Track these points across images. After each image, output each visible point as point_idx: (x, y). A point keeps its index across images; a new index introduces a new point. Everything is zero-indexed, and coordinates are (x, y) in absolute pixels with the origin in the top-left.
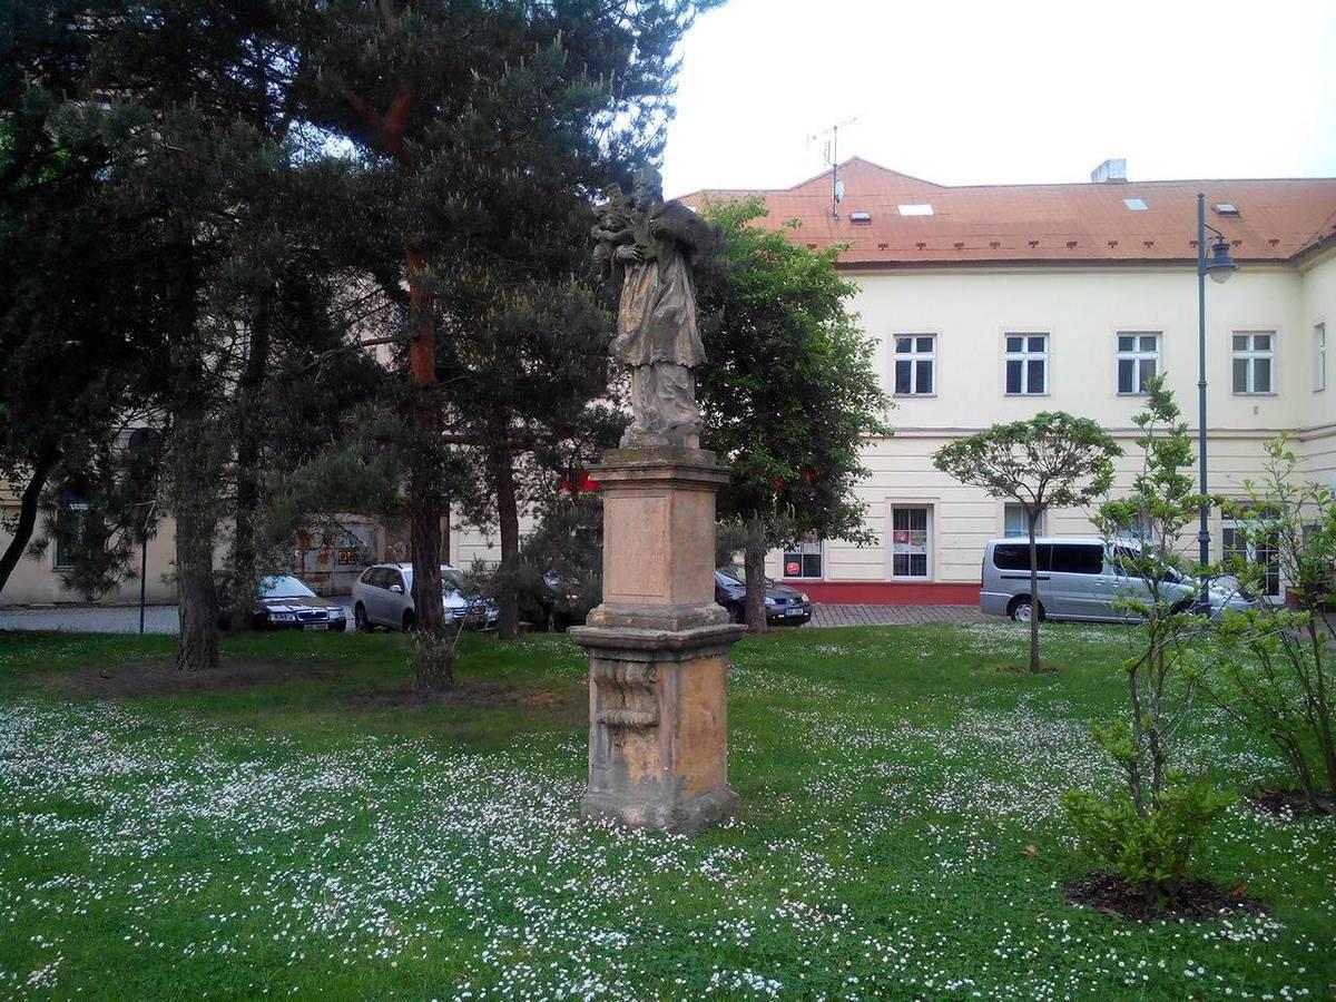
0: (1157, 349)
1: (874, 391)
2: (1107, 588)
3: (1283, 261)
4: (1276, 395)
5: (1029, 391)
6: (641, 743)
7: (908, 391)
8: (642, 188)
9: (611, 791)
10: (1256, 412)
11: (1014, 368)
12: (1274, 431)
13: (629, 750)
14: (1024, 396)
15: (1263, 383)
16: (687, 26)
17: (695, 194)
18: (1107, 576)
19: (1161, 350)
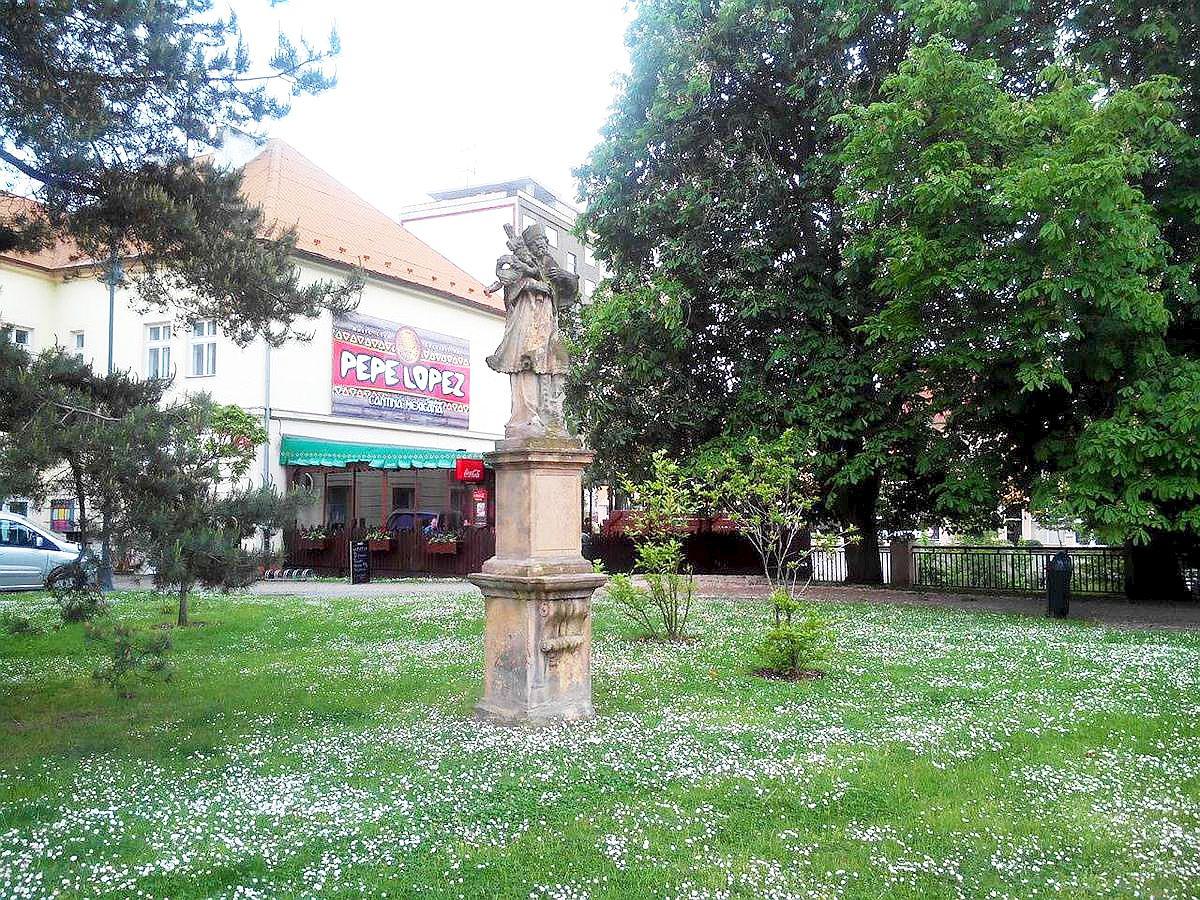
3: (48, 270)
13: (562, 667)
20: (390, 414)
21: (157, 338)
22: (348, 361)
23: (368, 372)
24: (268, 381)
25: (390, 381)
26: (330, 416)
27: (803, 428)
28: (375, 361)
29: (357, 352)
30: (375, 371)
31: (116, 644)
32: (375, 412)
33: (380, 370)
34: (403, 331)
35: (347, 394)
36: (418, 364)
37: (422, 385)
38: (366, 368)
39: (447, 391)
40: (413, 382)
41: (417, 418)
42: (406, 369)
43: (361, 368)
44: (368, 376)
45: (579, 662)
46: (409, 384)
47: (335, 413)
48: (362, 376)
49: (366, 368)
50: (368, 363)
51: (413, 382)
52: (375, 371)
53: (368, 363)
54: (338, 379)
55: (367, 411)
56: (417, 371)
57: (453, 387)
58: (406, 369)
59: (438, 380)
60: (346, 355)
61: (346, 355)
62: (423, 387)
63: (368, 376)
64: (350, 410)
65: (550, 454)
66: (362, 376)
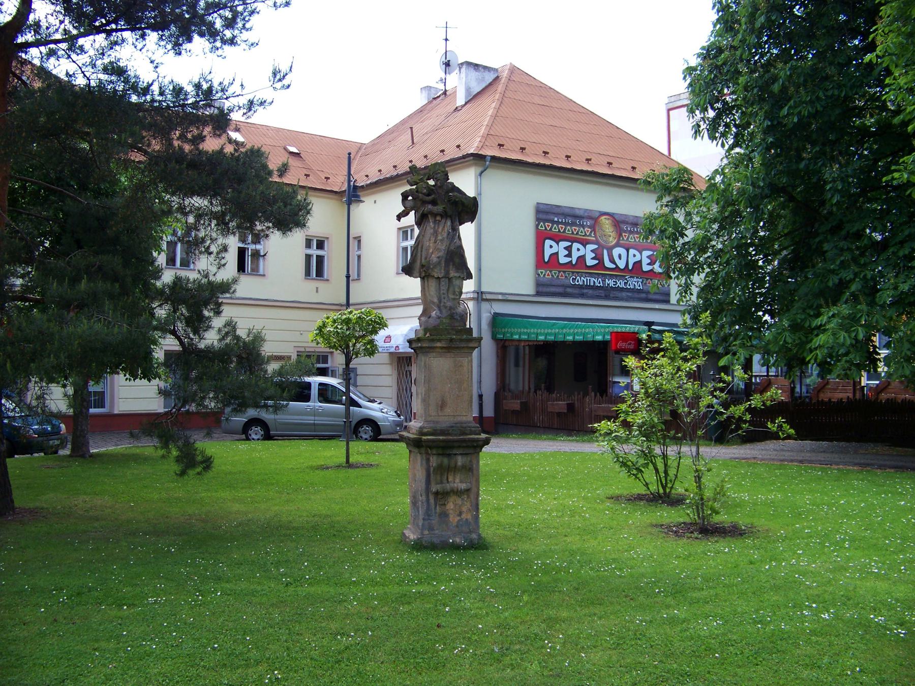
0: (326, 249)
1: (865, 294)
2: (314, 412)
3: (336, 192)
4: (328, 280)
5: (181, 266)
6: (459, 501)
7: (174, 265)
8: (442, 174)
9: (437, 532)
10: (317, 291)
11: (308, 257)
12: (330, 304)
13: (450, 506)
14: (178, 269)
15: (320, 273)
16: (684, 78)
17: (679, 164)
18: (315, 404)
19: (328, 248)
20: (590, 292)
21: (407, 239)
22: (550, 247)
23: (569, 255)
24: (480, 270)
25: (590, 262)
26: (533, 296)
27: (318, 332)
28: (576, 246)
29: (557, 239)
30: (575, 255)
31: (842, 596)
32: (566, 292)
33: (581, 253)
34: (603, 218)
35: (547, 275)
36: (618, 245)
37: (622, 265)
38: (567, 253)
39: (646, 268)
40: (612, 261)
41: (619, 294)
42: (605, 252)
43: (563, 253)
44: (569, 259)
45: (468, 504)
46: (608, 264)
47: (538, 294)
48: (563, 260)
49: (567, 253)
50: (569, 249)
51: (612, 261)
52: (575, 255)
53: (569, 249)
54: (539, 262)
55: (569, 290)
56: (616, 252)
57: (654, 264)
58: (605, 252)
59: (638, 258)
60: (548, 242)
61: (548, 242)
62: (622, 265)
63: (569, 259)
64: (553, 289)
65: (439, 340)
66: (563, 260)
